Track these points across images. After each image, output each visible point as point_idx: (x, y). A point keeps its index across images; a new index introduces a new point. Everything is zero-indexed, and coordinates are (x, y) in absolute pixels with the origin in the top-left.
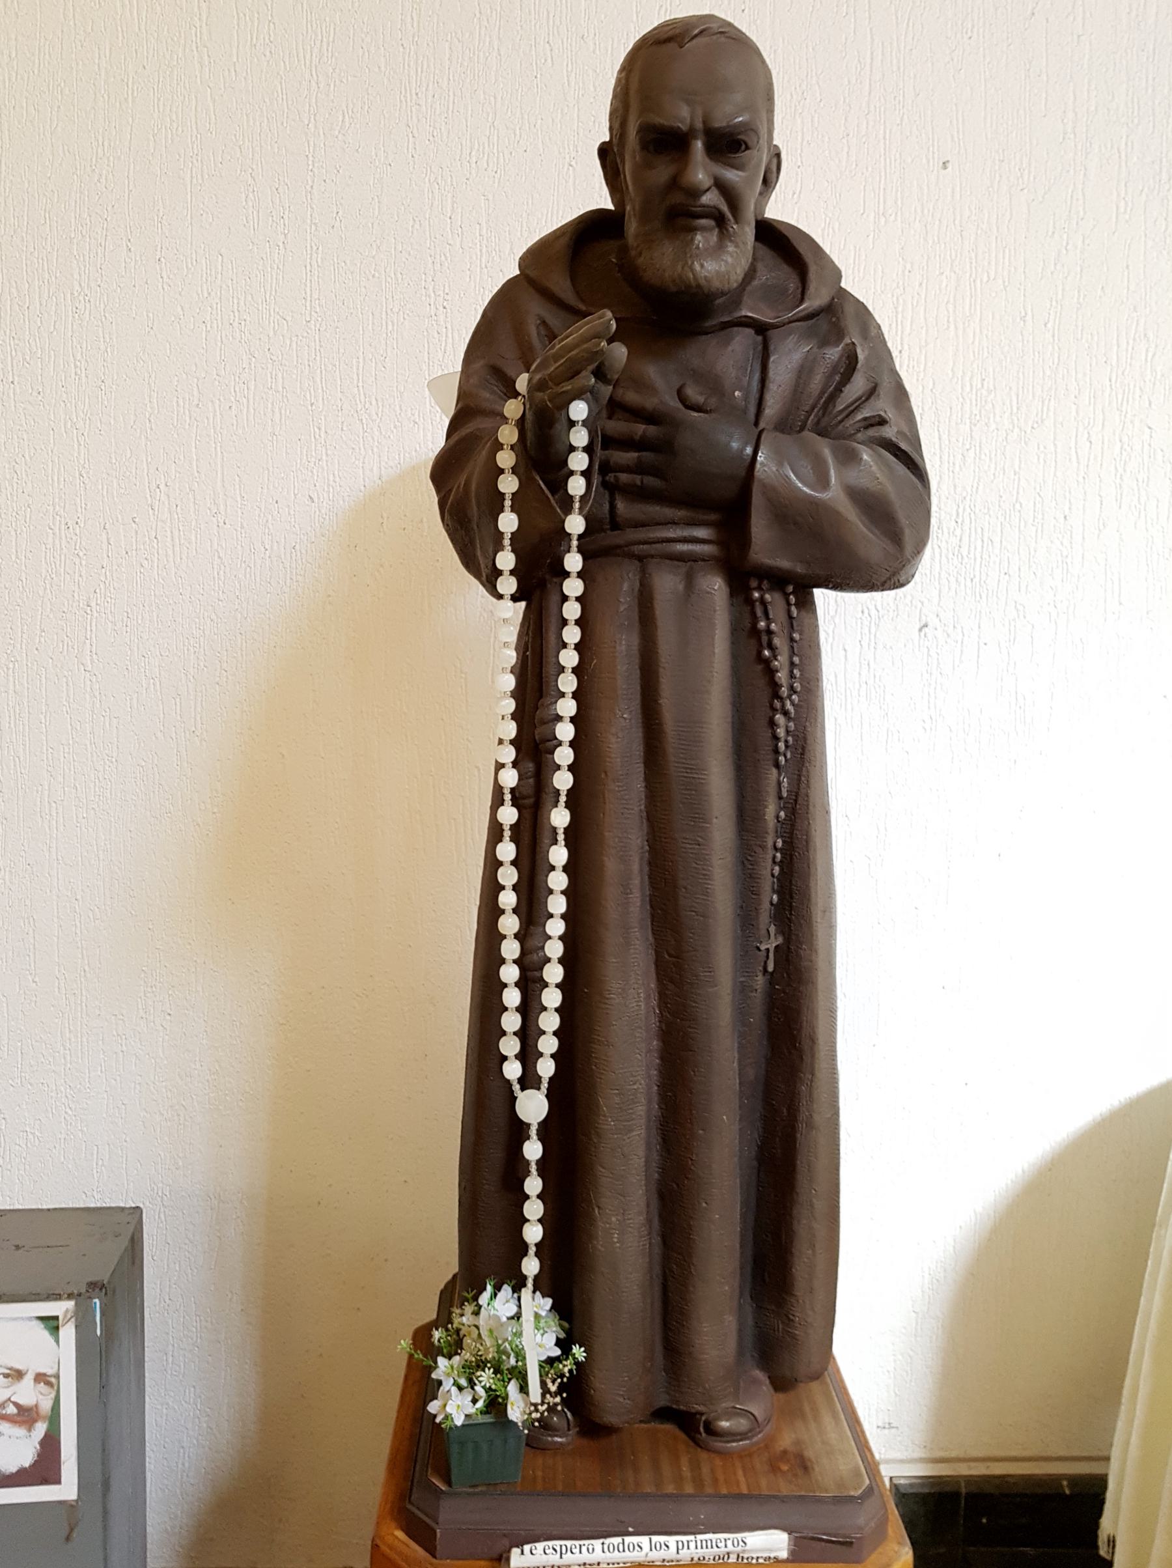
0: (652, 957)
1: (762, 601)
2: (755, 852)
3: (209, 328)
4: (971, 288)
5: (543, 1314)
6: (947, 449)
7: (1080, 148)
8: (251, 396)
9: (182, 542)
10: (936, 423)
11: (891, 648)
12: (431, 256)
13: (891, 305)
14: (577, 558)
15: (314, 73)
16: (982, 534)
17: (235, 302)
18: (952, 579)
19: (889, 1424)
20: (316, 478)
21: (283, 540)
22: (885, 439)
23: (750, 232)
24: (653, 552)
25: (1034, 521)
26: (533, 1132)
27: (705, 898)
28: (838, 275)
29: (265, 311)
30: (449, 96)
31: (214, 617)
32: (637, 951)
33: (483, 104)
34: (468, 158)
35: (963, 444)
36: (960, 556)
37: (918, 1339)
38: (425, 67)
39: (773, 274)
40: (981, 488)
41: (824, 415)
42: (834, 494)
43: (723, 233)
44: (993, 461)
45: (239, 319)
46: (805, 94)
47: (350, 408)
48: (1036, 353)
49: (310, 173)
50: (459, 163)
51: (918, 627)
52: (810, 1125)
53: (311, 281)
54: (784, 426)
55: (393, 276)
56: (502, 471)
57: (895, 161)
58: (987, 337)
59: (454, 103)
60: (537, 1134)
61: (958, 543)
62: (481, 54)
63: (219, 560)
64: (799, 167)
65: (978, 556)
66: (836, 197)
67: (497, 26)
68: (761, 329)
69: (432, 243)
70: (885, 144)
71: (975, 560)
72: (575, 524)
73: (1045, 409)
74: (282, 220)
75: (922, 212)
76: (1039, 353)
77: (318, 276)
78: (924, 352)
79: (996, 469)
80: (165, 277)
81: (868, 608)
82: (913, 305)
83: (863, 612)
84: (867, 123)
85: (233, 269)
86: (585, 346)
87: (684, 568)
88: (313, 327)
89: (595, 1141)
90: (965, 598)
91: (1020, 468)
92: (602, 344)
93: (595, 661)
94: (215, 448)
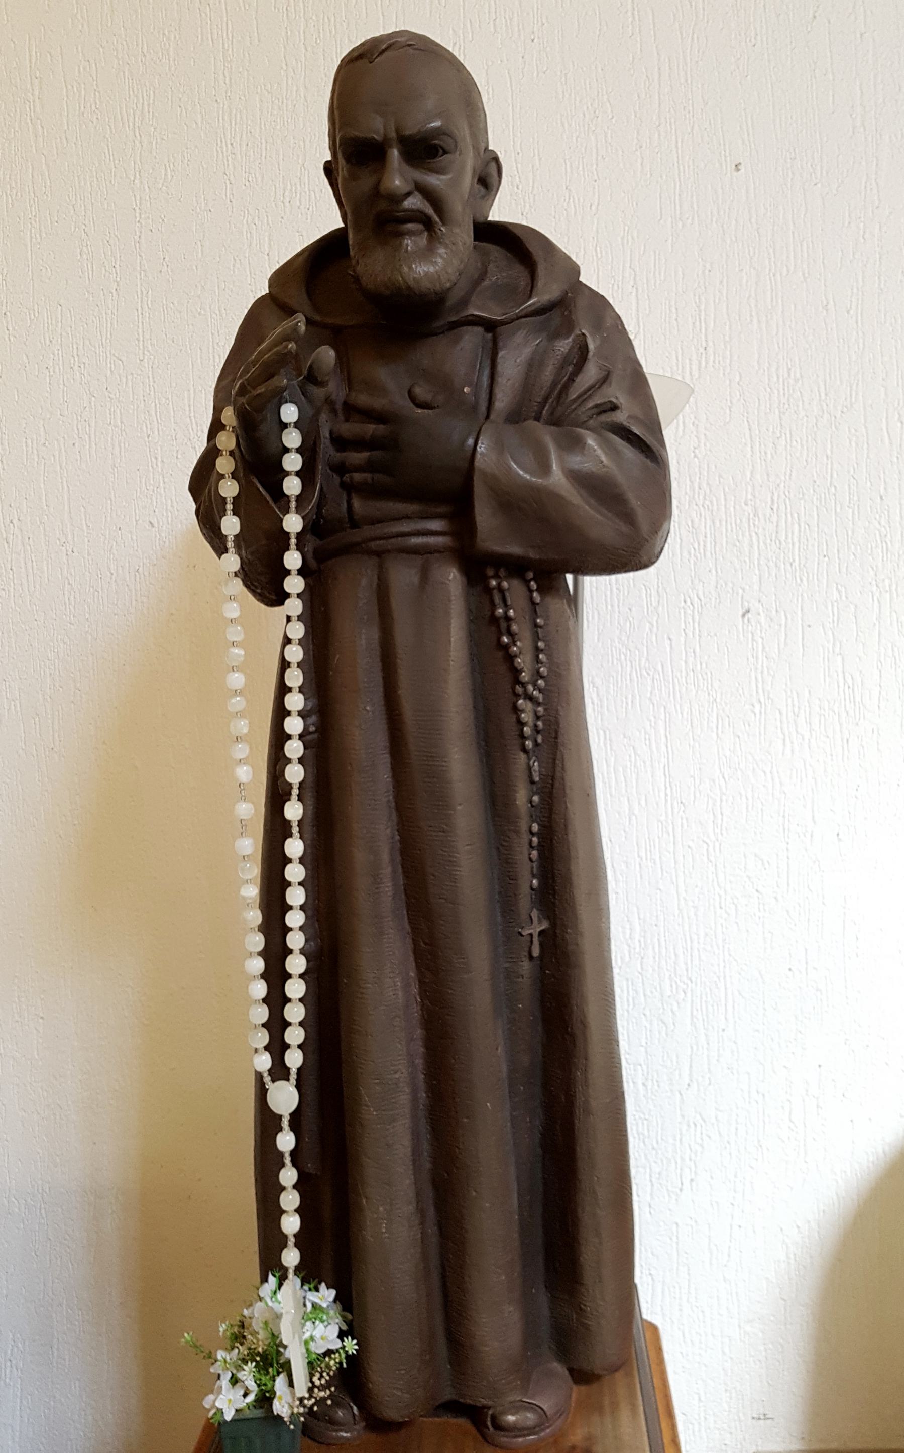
0: (410, 946)
1: (501, 591)
2: (509, 837)
3: (52, 373)
4: (771, 283)
5: (324, 1305)
6: (758, 439)
7: (870, 139)
8: (93, 433)
9: (35, 572)
10: (746, 414)
11: (716, 635)
12: (252, 291)
13: (694, 305)
14: (296, 556)
15: (137, 134)
16: (799, 520)
17: (75, 347)
18: (771, 564)
19: (765, 1415)
20: (155, 504)
21: (127, 565)
22: (617, 424)
23: (464, 235)
24: (389, 547)
25: (850, 503)
26: (285, 1123)
27: (453, 884)
28: (575, 270)
29: (102, 353)
30: (261, 143)
31: (66, 640)
32: (391, 940)
33: (293, 148)
34: (282, 199)
35: (774, 432)
36: (778, 542)
37: (789, 1327)
38: (238, 118)
39: (504, 274)
40: (794, 474)
41: (557, 406)
42: (557, 478)
43: (432, 235)
44: (805, 447)
45: (79, 363)
46: (597, 112)
47: (183, 437)
48: (841, 340)
49: (137, 224)
50: (273, 204)
51: (741, 613)
52: (588, 1112)
53: (143, 323)
54: (515, 417)
55: (218, 312)
56: (222, 476)
57: (689, 167)
58: (790, 327)
59: (266, 149)
60: (290, 1125)
61: (775, 529)
62: (290, 103)
63: (70, 586)
64: (595, 181)
65: (796, 540)
66: (633, 206)
67: (303, 77)
68: (490, 326)
69: (253, 280)
70: (677, 152)
71: (793, 544)
72: (293, 523)
73: (854, 394)
74: (114, 270)
75: (718, 213)
76: (843, 339)
77: (149, 318)
78: (729, 347)
79: (808, 455)
80: (11, 329)
81: (690, 597)
82: (714, 302)
83: (685, 602)
84: (659, 135)
85: (71, 317)
86: (275, 349)
87: (419, 560)
88: (146, 365)
89: (360, 1131)
90: (785, 582)
91: (832, 452)
92: (290, 346)
93: (338, 656)
94: (62, 482)
